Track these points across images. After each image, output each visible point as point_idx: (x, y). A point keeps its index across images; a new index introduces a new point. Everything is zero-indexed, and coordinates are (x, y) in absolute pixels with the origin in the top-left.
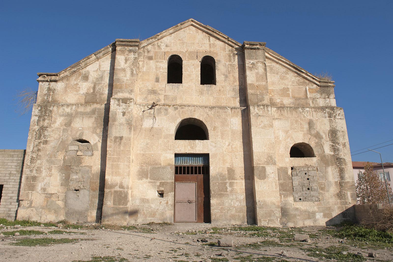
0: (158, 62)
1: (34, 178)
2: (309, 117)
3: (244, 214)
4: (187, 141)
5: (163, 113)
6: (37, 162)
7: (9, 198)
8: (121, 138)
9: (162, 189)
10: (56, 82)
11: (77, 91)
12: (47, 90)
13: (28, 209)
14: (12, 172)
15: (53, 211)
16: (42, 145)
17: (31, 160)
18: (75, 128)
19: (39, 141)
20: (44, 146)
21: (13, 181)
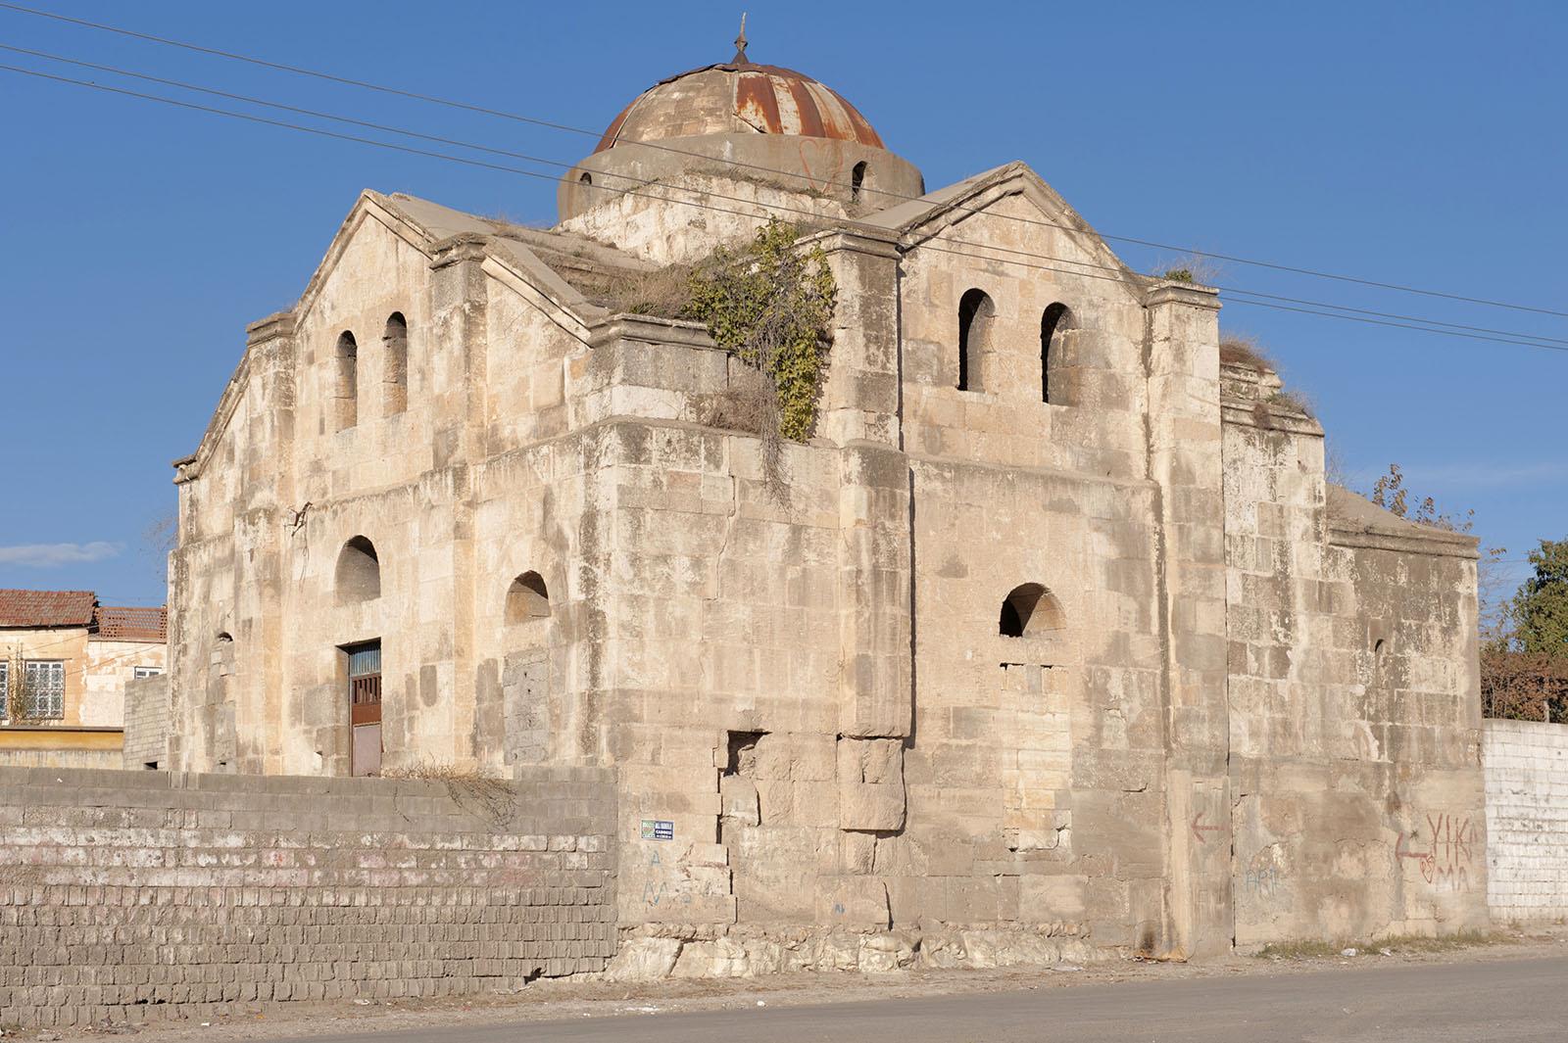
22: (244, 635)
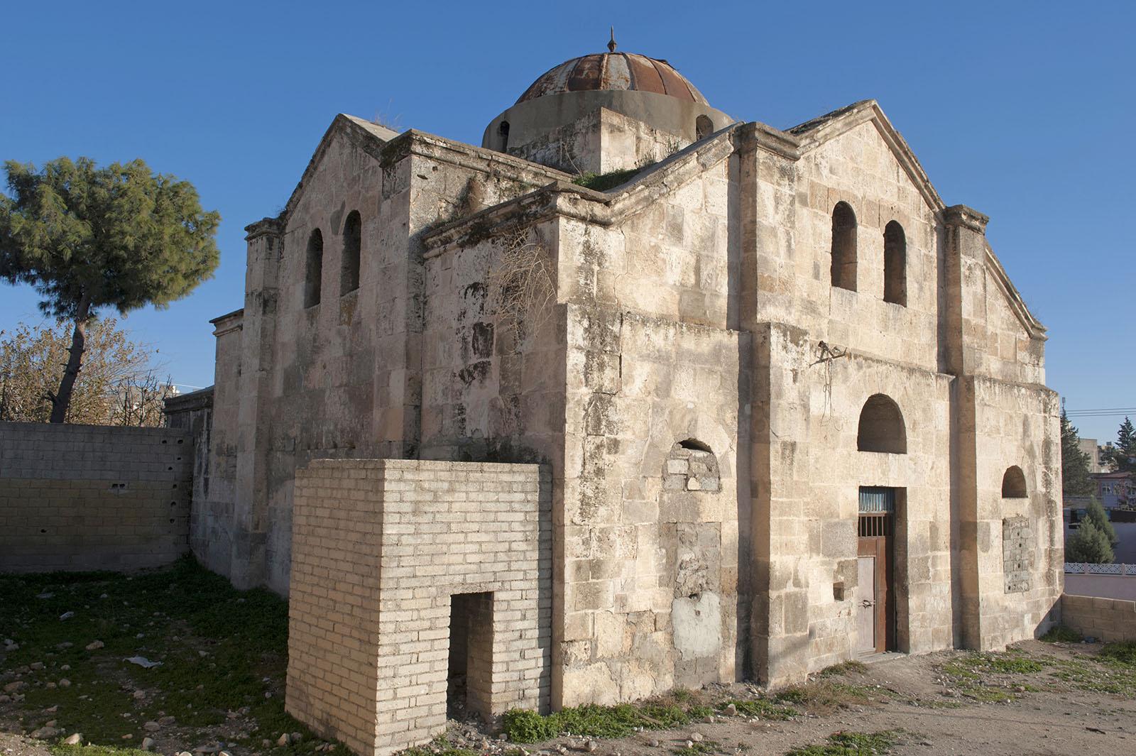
0: (816, 215)
1: (596, 567)
2: (1024, 410)
3: (947, 627)
4: (876, 453)
5: (840, 376)
6: (599, 513)
7: (517, 634)
8: (793, 445)
9: (841, 578)
10: (605, 228)
11: (660, 272)
12: (584, 252)
13: (589, 667)
14: (514, 546)
15: (647, 666)
16: (606, 456)
17: (582, 505)
18: (680, 405)
19: (598, 440)
20: (612, 458)
21: (521, 576)
22: (783, 458)
